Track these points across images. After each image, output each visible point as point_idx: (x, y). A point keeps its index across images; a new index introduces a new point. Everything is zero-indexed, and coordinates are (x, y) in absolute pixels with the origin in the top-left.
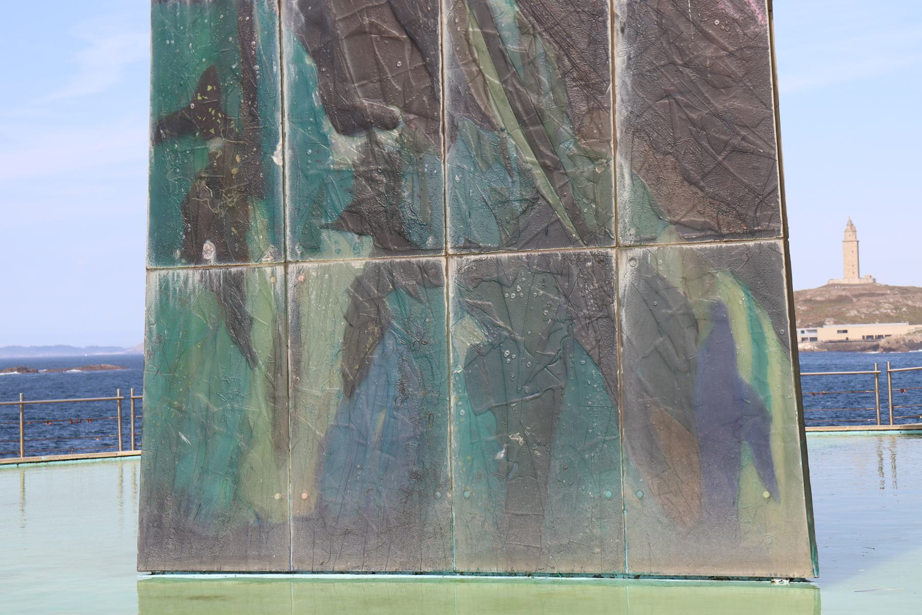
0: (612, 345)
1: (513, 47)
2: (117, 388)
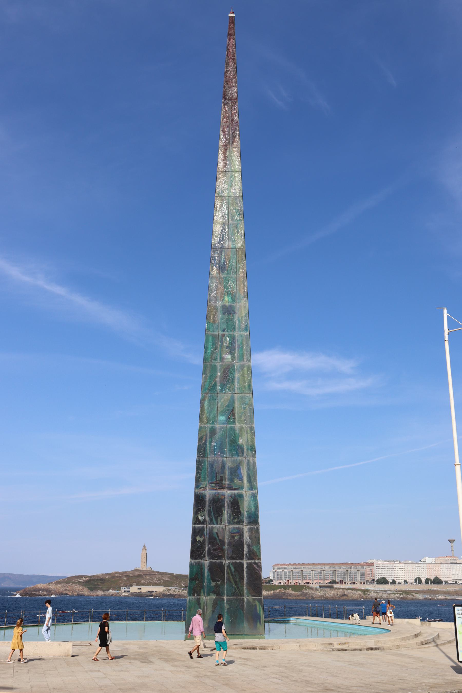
0: (244, 608)
1: (234, 573)
2: (56, 609)
